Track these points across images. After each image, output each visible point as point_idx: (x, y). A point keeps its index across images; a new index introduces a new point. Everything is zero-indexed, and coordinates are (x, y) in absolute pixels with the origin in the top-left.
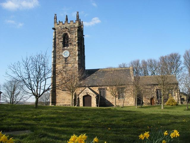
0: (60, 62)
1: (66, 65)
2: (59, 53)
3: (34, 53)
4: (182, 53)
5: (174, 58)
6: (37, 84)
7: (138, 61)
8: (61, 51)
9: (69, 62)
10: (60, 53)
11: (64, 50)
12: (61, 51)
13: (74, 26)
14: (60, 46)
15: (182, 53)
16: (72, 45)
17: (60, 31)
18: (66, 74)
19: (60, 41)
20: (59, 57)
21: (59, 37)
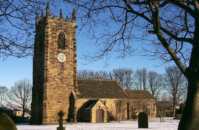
0: (54, 67)
1: (61, 72)
2: (53, 55)
3: (22, 78)
4: (134, 70)
5: (129, 72)
6: (29, 47)
7: (144, 71)
8: (55, 53)
9: (65, 68)
10: (55, 56)
11: (59, 52)
12: (55, 53)
13: (71, 26)
14: (55, 46)
15: (134, 70)
16: (69, 48)
17: (54, 28)
18: (61, 82)
19: (54, 40)
20: (54, 61)
21: (54, 35)
